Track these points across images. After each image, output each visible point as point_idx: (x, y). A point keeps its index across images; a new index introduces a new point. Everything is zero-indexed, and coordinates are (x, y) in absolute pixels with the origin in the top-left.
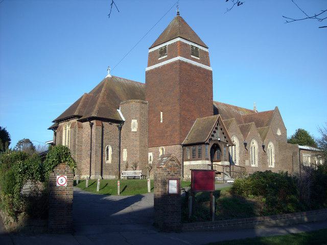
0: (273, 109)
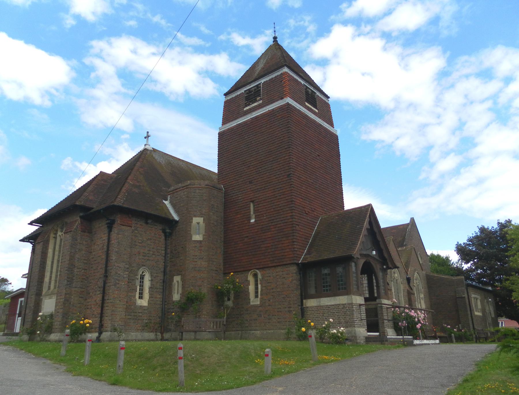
0: (408, 221)
